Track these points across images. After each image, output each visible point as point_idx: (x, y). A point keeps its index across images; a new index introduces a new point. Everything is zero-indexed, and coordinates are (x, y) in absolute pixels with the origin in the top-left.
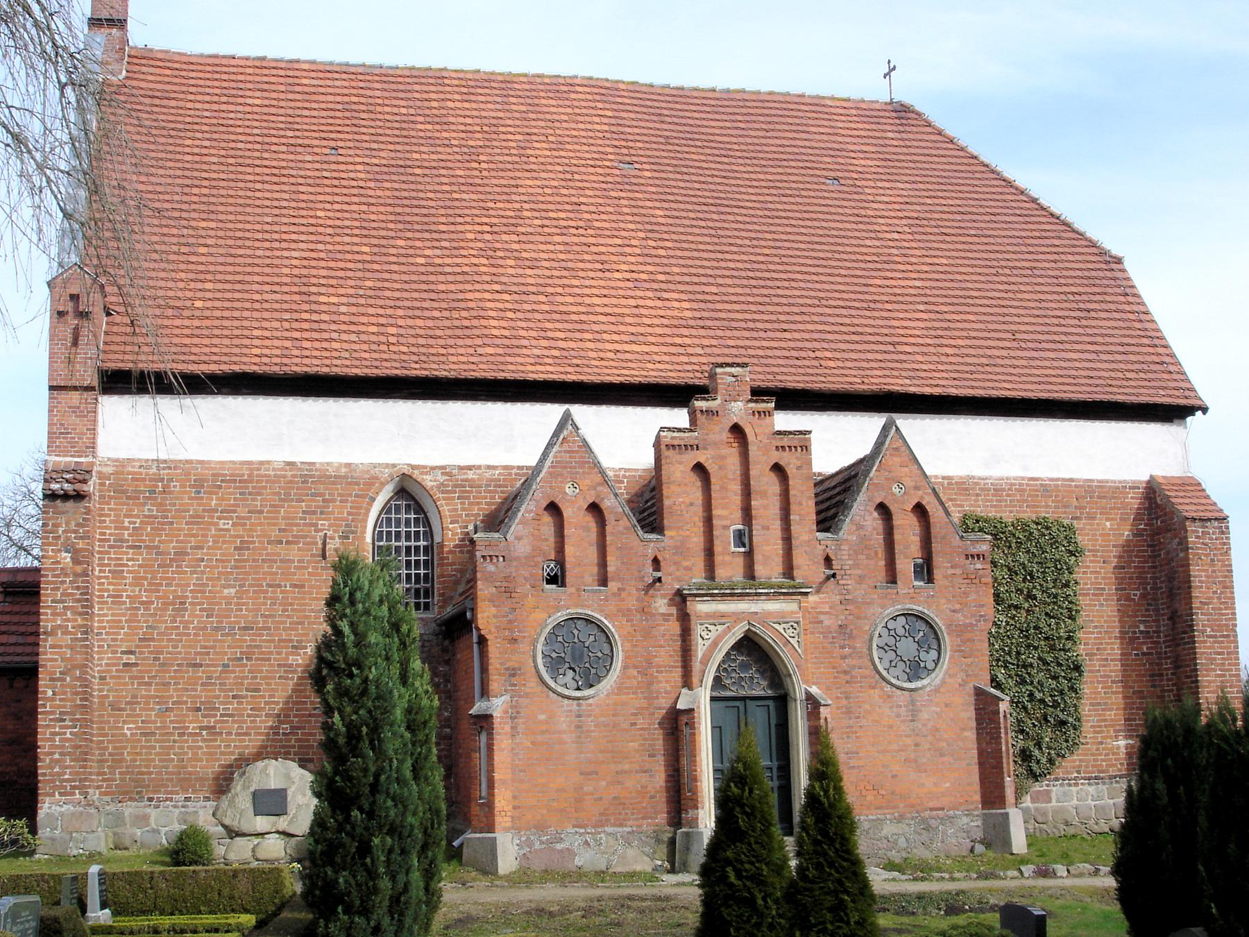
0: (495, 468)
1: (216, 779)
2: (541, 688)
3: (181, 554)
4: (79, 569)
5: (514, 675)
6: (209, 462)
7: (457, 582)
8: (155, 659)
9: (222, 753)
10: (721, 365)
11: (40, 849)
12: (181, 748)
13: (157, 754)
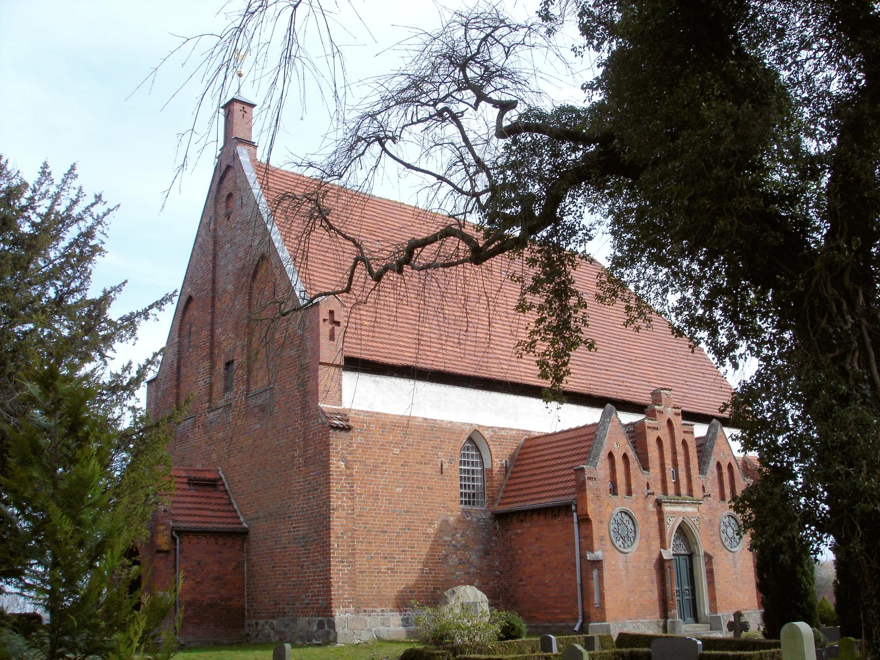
0: (513, 430)
1: (396, 599)
2: (612, 547)
3: (376, 467)
4: (348, 472)
5: (602, 540)
6: (388, 415)
7: (499, 491)
8: (365, 527)
9: (398, 584)
10: (663, 389)
11: (339, 639)
12: (379, 580)
13: (368, 584)
